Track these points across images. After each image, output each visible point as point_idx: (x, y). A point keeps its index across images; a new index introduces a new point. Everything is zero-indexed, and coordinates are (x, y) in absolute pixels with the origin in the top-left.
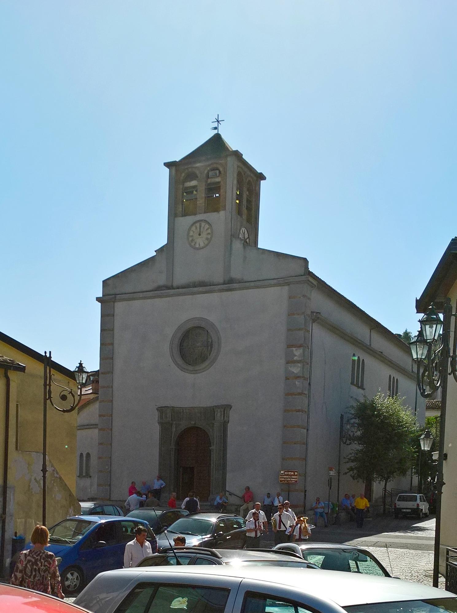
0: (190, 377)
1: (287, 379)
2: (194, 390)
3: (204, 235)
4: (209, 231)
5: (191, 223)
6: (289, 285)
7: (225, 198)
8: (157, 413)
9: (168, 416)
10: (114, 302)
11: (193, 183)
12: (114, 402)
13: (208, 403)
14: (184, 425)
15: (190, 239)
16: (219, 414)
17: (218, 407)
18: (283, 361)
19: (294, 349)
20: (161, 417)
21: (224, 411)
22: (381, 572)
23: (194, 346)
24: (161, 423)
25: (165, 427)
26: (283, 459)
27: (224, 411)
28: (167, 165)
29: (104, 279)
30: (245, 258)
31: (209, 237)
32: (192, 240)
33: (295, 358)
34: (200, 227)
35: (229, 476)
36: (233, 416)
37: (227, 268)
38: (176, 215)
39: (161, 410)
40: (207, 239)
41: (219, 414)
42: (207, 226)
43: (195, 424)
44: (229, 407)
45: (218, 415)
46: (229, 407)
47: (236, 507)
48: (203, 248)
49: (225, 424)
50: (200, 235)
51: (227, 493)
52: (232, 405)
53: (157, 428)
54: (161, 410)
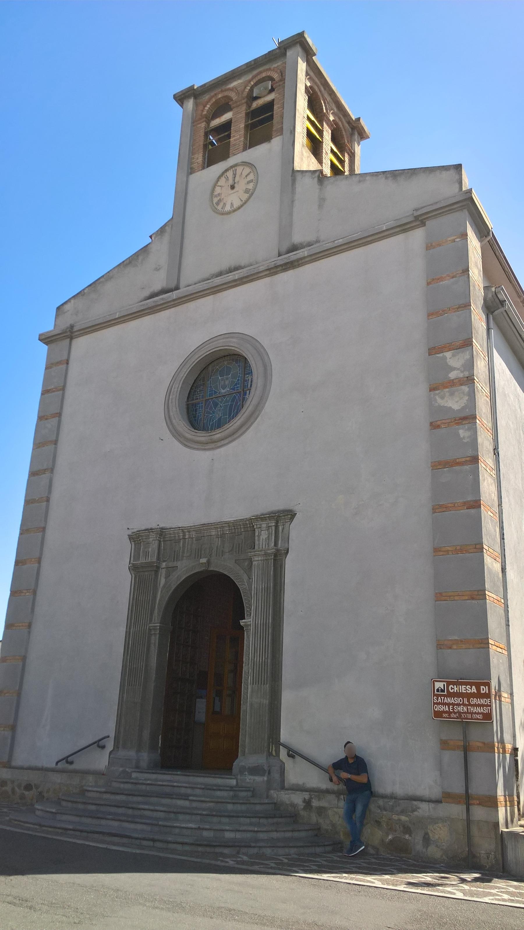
0: (203, 457)
1: (434, 426)
2: (208, 487)
3: (241, 186)
4: (251, 177)
5: (221, 172)
6: (423, 224)
7: (282, 117)
8: (127, 547)
9: (151, 549)
10: (71, 338)
11: (228, 116)
12: (49, 533)
13: (236, 511)
14: (185, 568)
15: (215, 200)
16: (264, 535)
17: (261, 518)
18: (422, 390)
19: (448, 354)
20: (136, 554)
21: (277, 527)
22: (490, 425)
23: (215, 392)
24: (134, 568)
25: (143, 574)
26: (440, 646)
27: (277, 527)
28: (181, 98)
29: (57, 306)
30: (322, 201)
31: (251, 186)
32: (220, 201)
33: (453, 375)
34: (235, 175)
35: (287, 697)
36: (296, 531)
37: (285, 228)
38: (191, 171)
39: (137, 538)
40: (247, 191)
41: (264, 535)
42: (247, 170)
43: (209, 562)
44: (290, 515)
45: (263, 536)
46: (290, 515)
47: (306, 796)
48: (239, 208)
49: (278, 558)
50: (233, 187)
51: (283, 752)
52: (296, 509)
53: (125, 580)
54: (137, 538)
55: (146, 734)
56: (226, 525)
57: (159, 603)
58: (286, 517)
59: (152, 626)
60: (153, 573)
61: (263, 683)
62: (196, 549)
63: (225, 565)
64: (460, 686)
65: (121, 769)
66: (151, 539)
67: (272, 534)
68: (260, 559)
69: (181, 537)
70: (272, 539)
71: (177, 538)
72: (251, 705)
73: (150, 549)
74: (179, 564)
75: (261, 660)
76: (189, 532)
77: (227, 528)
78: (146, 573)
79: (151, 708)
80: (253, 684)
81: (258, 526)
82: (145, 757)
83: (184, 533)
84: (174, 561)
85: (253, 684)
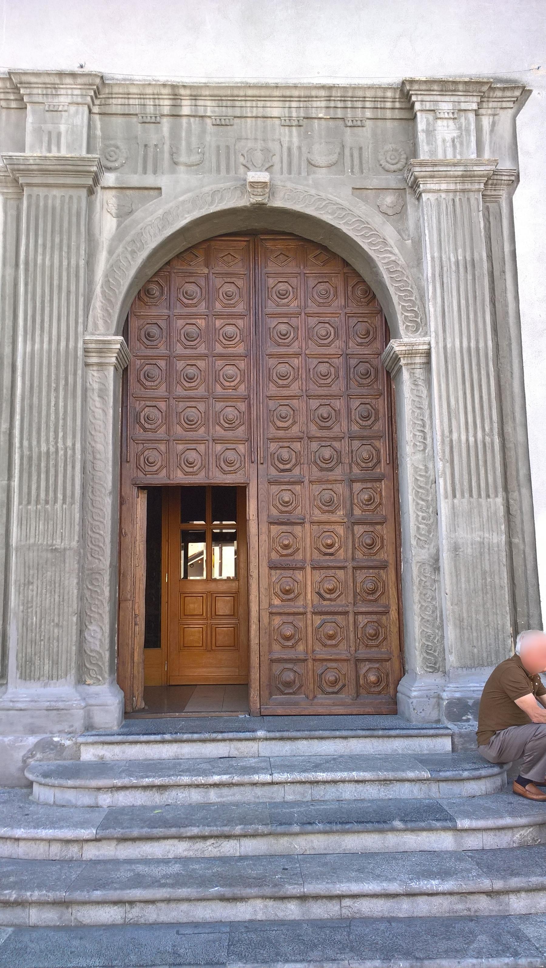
55: (99, 636)
56: (322, 93)
57: (107, 282)
58: (508, 93)
59: (92, 341)
60: (84, 193)
61: (483, 494)
62: (218, 147)
63: (319, 194)
64: (217, 549)
65: (32, 740)
66: (64, 100)
67: (468, 131)
68: (444, 186)
69: (166, 110)
70: (469, 142)
71: (150, 109)
72: (456, 549)
73: (63, 128)
74: (163, 181)
75: (471, 439)
76: (195, 97)
77: (323, 104)
78: (56, 192)
79: (108, 563)
80: (454, 496)
81: (428, 106)
82: (107, 701)
83: (176, 97)
84: (145, 172)
85: (454, 496)
